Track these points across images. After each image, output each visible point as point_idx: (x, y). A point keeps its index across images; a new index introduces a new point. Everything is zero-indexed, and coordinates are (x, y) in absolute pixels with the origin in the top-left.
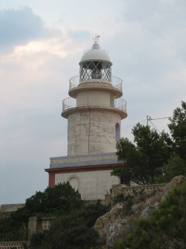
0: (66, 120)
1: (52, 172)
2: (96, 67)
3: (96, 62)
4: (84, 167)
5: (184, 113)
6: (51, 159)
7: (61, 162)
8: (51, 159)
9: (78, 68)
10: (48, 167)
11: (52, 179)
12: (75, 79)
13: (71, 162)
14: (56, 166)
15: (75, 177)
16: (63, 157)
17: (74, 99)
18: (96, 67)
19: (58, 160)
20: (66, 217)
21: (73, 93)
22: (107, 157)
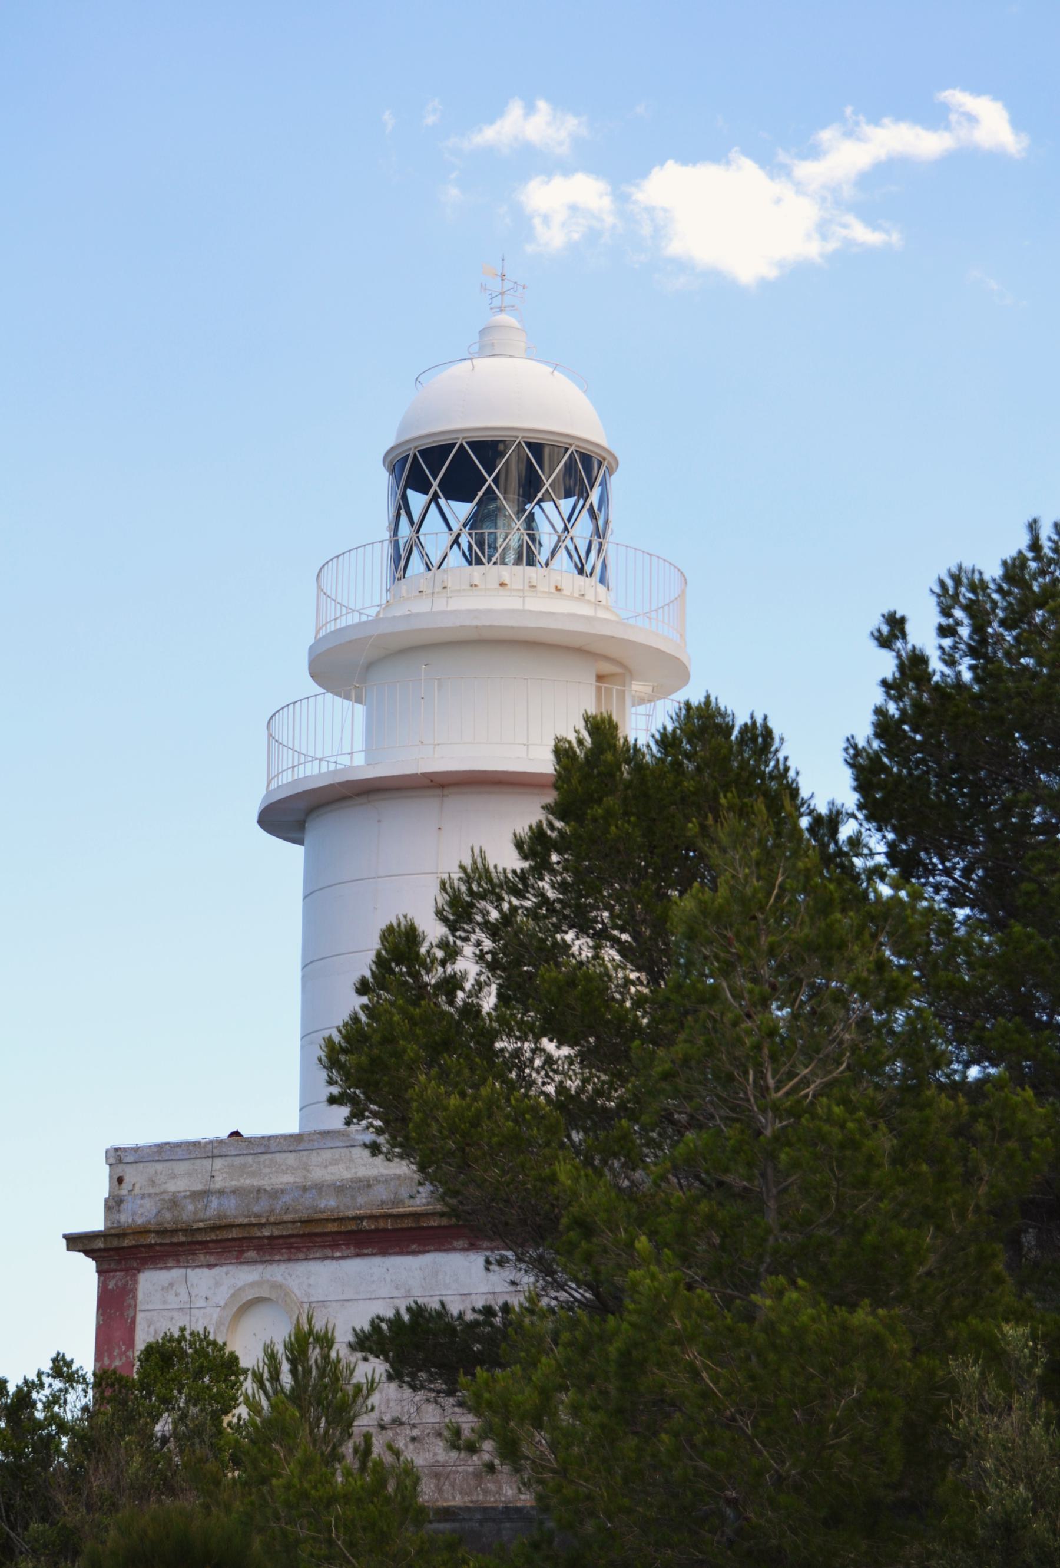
0: (289, 858)
1: (119, 1253)
2: (490, 480)
3: (489, 449)
4: (332, 1228)
5: (708, 1049)
6: (117, 1157)
7: (181, 1181)
8: (117, 1157)
9: (378, 486)
10: (95, 1222)
11: (114, 1309)
12: (340, 567)
13: (247, 1182)
14: (141, 1212)
15: (269, 1299)
16: (196, 1144)
17: (346, 702)
18: (490, 480)
19: (159, 1167)
20: (892, 957)
21: (345, 665)
22: (318, 1255)
